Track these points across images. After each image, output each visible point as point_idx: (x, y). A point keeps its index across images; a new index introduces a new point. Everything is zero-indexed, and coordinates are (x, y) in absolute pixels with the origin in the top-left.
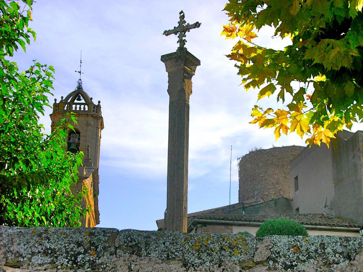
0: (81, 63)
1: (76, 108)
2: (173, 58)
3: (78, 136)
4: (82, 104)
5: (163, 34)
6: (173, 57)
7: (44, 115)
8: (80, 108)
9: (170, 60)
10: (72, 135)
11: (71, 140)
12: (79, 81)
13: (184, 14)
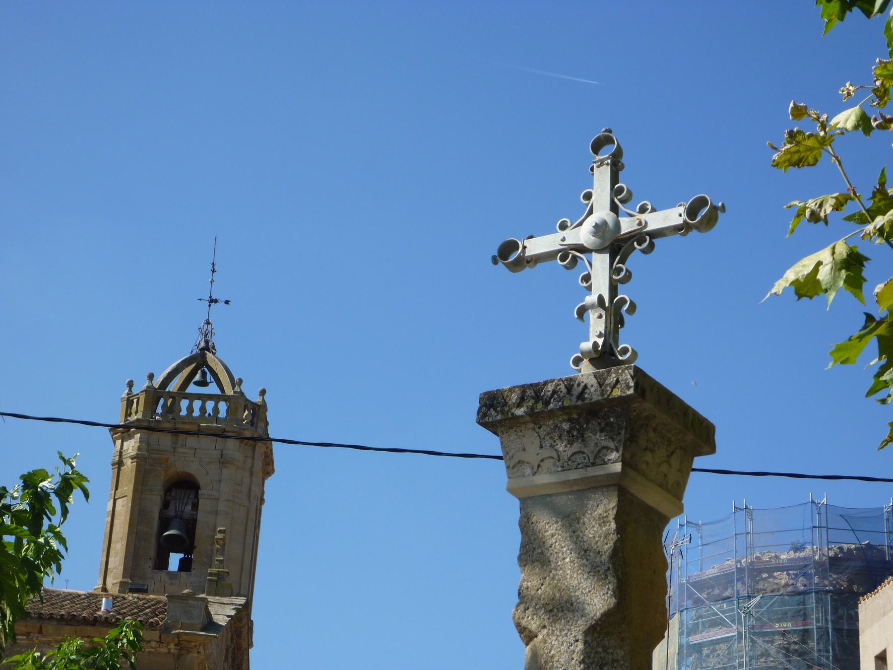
0: (213, 271)
1: (190, 409)
2: (551, 414)
3: (192, 496)
4: (210, 397)
5: (495, 261)
6: (551, 406)
7: (59, 453)
8: (203, 409)
9: (534, 422)
10: (173, 494)
11: (172, 506)
12: (206, 325)
13: (112, 436)
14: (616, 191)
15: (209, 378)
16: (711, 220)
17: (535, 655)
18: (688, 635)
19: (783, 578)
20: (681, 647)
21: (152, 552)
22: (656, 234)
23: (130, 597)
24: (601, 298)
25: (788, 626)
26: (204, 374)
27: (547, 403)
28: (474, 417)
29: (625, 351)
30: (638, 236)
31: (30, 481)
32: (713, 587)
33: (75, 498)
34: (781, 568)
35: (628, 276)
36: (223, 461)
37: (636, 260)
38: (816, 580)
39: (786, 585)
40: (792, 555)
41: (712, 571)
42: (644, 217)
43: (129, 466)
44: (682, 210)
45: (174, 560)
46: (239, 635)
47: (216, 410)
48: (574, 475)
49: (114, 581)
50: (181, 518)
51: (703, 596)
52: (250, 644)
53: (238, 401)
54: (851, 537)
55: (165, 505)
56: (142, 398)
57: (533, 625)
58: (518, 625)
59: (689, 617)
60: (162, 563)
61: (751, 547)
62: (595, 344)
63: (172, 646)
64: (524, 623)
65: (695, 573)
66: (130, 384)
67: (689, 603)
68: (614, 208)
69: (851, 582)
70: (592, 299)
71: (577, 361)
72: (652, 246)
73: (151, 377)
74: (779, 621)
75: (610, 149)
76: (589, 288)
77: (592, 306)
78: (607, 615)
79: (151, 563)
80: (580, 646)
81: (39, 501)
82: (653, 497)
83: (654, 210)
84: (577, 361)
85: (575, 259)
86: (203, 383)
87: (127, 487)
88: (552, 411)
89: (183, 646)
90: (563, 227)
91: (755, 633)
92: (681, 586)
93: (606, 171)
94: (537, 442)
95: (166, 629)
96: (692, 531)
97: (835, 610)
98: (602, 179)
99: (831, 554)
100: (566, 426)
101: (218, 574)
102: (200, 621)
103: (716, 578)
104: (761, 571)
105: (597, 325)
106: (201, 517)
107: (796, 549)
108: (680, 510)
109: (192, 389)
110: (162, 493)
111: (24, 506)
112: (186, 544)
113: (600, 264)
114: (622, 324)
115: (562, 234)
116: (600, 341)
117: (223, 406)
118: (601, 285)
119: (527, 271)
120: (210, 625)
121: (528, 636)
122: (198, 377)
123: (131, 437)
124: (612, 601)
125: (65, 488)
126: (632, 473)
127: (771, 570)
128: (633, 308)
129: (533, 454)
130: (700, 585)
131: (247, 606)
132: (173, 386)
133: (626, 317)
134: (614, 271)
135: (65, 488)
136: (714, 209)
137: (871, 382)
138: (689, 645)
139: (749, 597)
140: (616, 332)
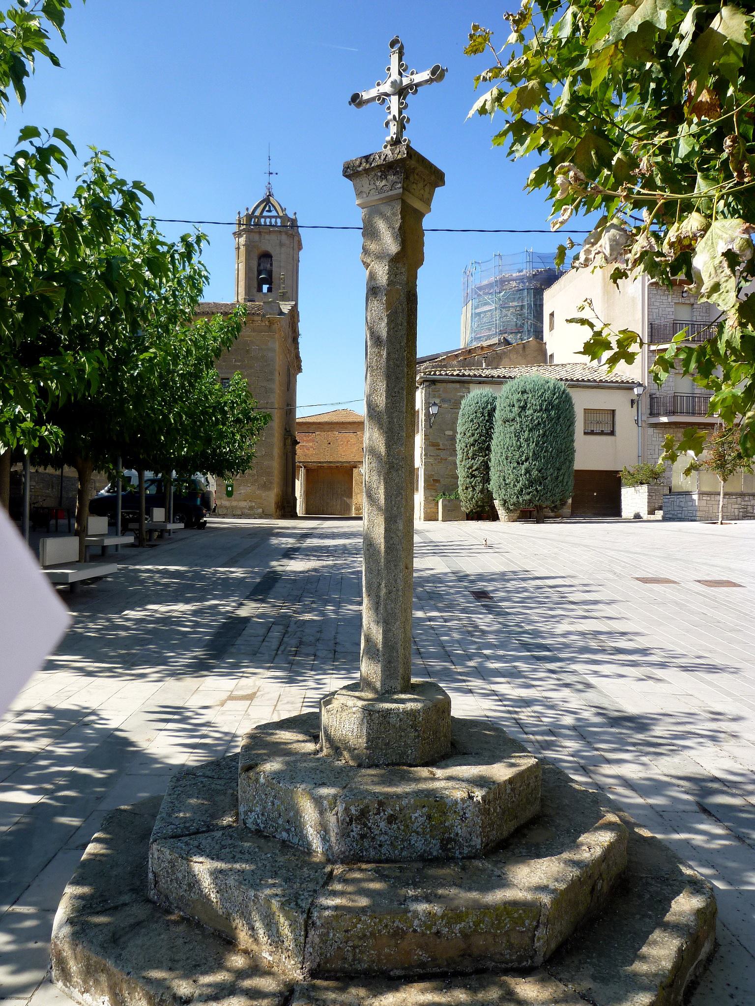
4: (273, 217)
11: (262, 265)
14: (400, 66)
15: (272, 208)
16: (441, 77)
17: (371, 273)
18: (475, 309)
19: (514, 284)
20: (472, 314)
21: (256, 285)
22: (418, 85)
23: (249, 304)
24: (394, 117)
25: (515, 304)
26: (270, 207)
27: (371, 164)
28: (342, 173)
29: (405, 140)
30: (410, 86)
31: (184, 239)
32: (485, 289)
33: (203, 244)
34: (513, 280)
35: (406, 106)
36: (281, 245)
37: (410, 98)
38: (527, 284)
39: (515, 287)
40: (518, 274)
41: (485, 282)
42: (412, 77)
43: (242, 249)
44: (428, 72)
45: (265, 288)
46: (294, 317)
47: (276, 222)
48: (383, 195)
49: (241, 298)
50: (266, 270)
51: (481, 293)
52: (299, 321)
53: (285, 218)
54: (542, 265)
55: (259, 265)
56: (245, 218)
57: (368, 261)
58: (363, 261)
59: (475, 302)
60: (260, 289)
61: (501, 272)
62: (392, 138)
63: (267, 323)
64: (365, 260)
65: (478, 284)
66: (239, 213)
67: (476, 296)
68: (400, 74)
69: (541, 285)
70: (390, 117)
71: (386, 147)
72: (416, 91)
73: (247, 209)
74: (512, 302)
75: (399, 45)
76: (390, 113)
77: (391, 120)
78: (397, 254)
79: (256, 290)
80: (387, 267)
81: (189, 246)
82: (417, 205)
83: (417, 73)
84: (386, 147)
85: (384, 99)
86: (269, 211)
87: (243, 258)
88: (373, 167)
89: (271, 322)
90: (379, 85)
91: (502, 307)
92: (472, 289)
93: (396, 56)
94: (368, 183)
95: (264, 316)
96: (477, 265)
97: (535, 296)
98: (395, 58)
99: (534, 273)
100: (379, 174)
101: (283, 293)
102: (277, 312)
103: (486, 285)
104: (505, 281)
105: (393, 129)
106: (275, 269)
107: (520, 271)
108: (430, 210)
109: (265, 214)
110: (257, 260)
111: (183, 250)
112: (269, 281)
113: (394, 100)
114: (405, 129)
115: (378, 88)
116: (395, 136)
117: (279, 221)
118: (395, 111)
119: (365, 108)
120: (281, 313)
121: (367, 265)
122: (267, 208)
123: (242, 236)
124: (399, 248)
125: (199, 240)
126: (407, 193)
127: (509, 281)
128: (408, 120)
129: (366, 189)
130: (480, 288)
131: (296, 305)
132: (257, 213)
133: (406, 124)
134: (400, 103)
135: (199, 240)
136: (443, 70)
137: (509, 150)
138: (476, 314)
139: (500, 292)
140: (402, 131)
